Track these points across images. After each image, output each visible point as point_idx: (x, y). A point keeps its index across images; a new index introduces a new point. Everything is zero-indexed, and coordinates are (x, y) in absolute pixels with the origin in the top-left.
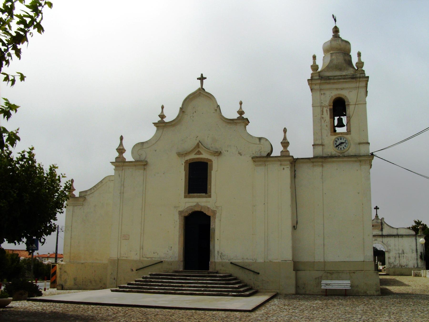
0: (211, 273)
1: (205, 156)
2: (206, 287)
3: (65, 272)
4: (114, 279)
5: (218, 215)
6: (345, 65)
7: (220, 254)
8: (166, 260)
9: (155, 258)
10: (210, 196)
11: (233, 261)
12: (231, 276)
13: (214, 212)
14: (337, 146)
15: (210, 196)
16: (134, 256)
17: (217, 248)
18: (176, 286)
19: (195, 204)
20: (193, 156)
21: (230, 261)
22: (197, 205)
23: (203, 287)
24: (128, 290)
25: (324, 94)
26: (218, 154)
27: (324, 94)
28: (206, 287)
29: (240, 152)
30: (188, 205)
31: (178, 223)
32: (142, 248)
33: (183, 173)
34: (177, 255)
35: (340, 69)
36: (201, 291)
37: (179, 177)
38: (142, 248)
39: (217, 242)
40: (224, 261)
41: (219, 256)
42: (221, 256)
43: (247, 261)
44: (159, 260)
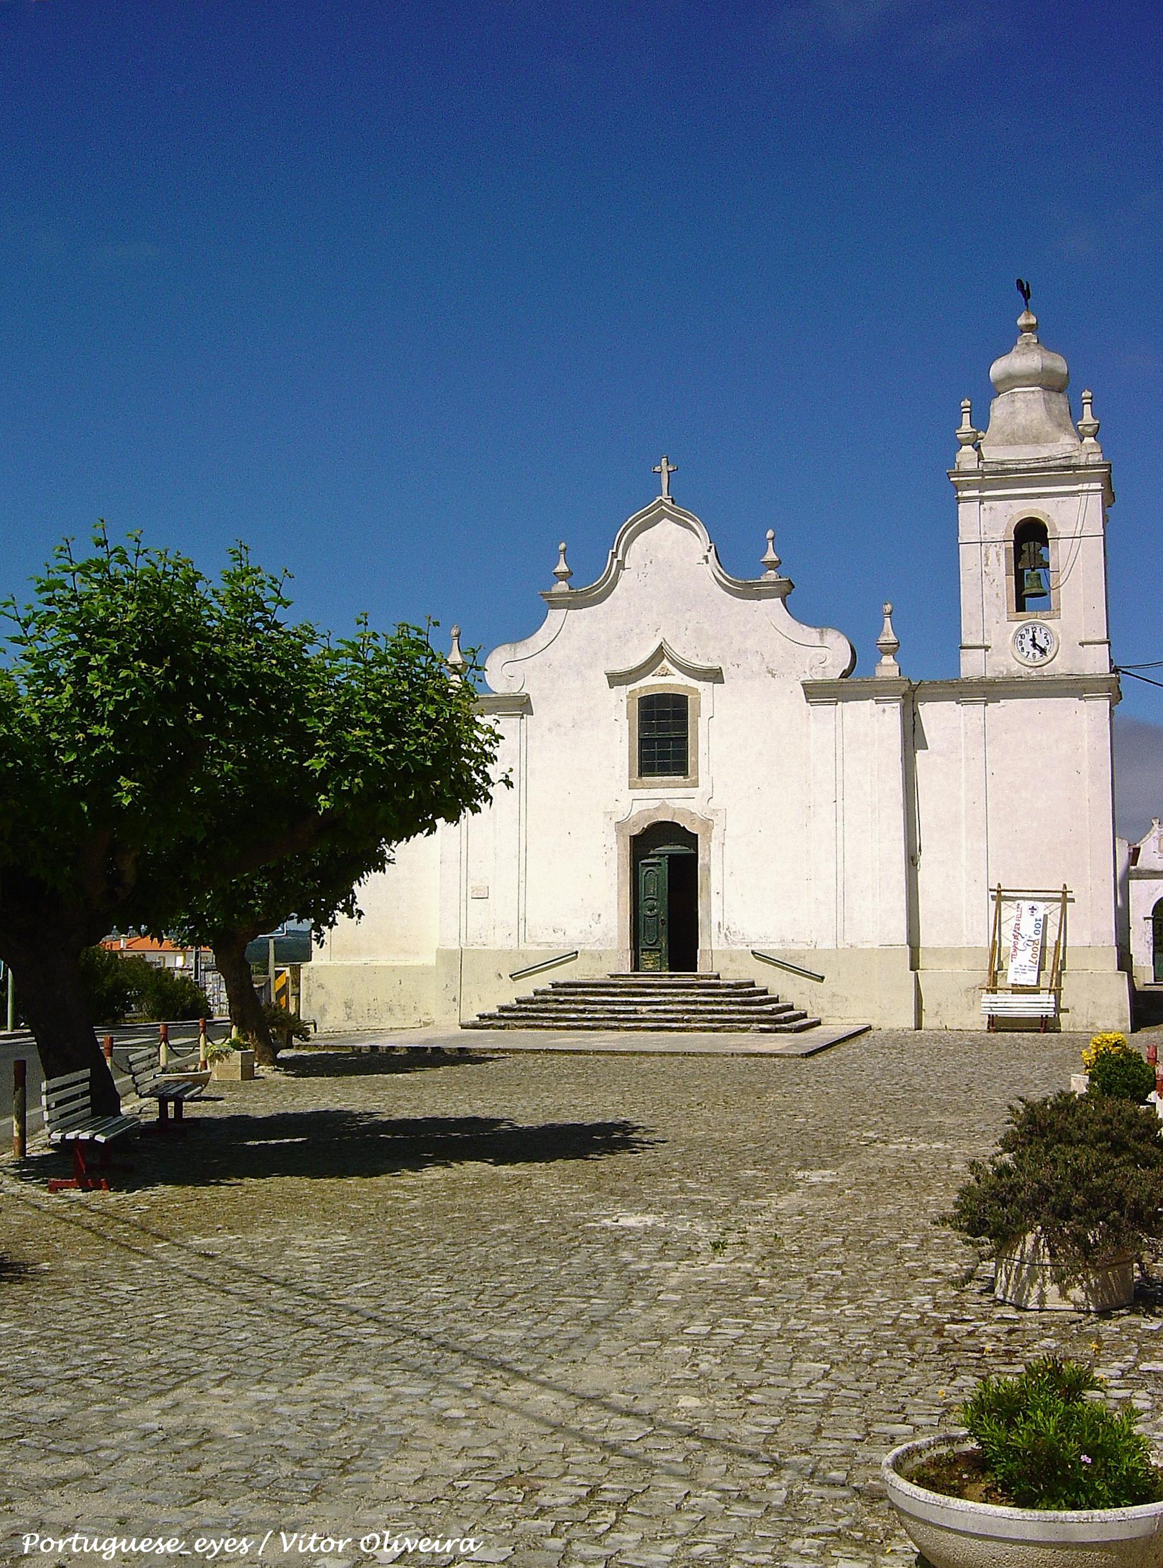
0: (702, 977)
1: (672, 680)
2: (694, 1012)
3: (321, 986)
4: (454, 1000)
5: (715, 832)
6: (1049, 427)
7: (723, 931)
8: (588, 948)
9: (559, 944)
10: (695, 785)
11: (756, 948)
12: (752, 984)
13: (707, 824)
14: (987, 648)
15: (695, 785)
16: (499, 941)
17: (716, 917)
18: (619, 1012)
19: (657, 803)
20: (651, 683)
21: (750, 948)
22: (663, 807)
23: (688, 1012)
24: (565, 1024)
25: (991, 509)
26: (715, 676)
27: (991, 509)
28: (694, 1012)
29: (771, 666)
30: (638, 807)
31: (614, 855)
32: (522, 920)
33: (626, 724)
34: (614, 933)
35: (1036, 440)
36: (683, 1021)
37: (616, 735)
38: (522, 920)
39: (715, 901)
40: (735, 948)
41: (722, 936)
42: (726, 935)
43: (794, 947)
44: (569, 949)
